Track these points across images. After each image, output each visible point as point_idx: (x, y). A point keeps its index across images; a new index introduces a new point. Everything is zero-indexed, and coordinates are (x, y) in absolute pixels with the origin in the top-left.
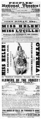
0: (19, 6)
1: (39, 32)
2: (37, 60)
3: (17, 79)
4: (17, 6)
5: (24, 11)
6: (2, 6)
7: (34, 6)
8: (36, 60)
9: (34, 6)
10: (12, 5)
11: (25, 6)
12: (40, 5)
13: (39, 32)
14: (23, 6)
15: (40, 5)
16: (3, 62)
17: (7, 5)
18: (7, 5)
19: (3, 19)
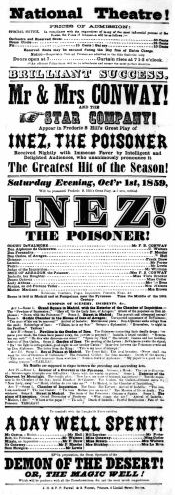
0: (80, 16)
1: (166, 103)
2: (107, 15)
3: (108, 419)
4: (75, 17)
5: (75, 487)
6: (10, 13)
7: (145, 15)
8: (107, 19)
9: (145, 15)
10: (50, 17)
11: (105, 14)
12: (167, 12)
13: (166, 103)
14: (98, 14)
15: (167, 12)
16: (6, 422)
17: (33, 11)
18: (33, 11)
19: (34, 57)
